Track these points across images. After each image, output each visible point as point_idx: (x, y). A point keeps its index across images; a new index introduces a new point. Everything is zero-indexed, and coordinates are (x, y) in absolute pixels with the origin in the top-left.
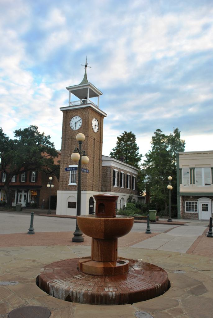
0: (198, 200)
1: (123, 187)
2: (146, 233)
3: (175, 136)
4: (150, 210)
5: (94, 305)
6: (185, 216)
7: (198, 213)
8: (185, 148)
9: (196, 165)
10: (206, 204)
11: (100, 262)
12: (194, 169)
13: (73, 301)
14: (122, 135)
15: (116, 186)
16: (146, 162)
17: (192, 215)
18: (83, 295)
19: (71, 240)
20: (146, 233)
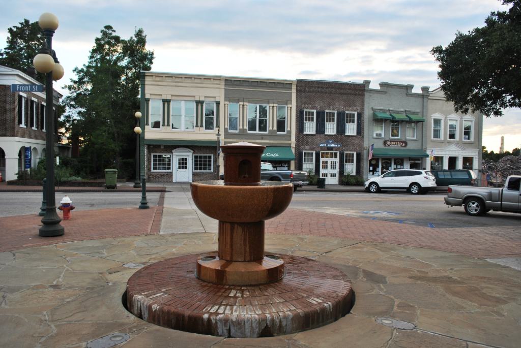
0: (173, 151)
1: (34, 128)
2: (141, 208)
3: (138, 42)
4: (107, 170)
5: (308, 331)
6: (151, 177)
7: (172, 173)
8: (152, 66)
9: (172, 96)
10: (184, 157)
11: (248, 261)
12: (168, 101)
13: (274, 334)
14: (20, 26)
15: (23, 125)
16: (75, 82)
17: (162, 174)
18: (292, 319)
19: (38, 232)
20: (141, 208)
